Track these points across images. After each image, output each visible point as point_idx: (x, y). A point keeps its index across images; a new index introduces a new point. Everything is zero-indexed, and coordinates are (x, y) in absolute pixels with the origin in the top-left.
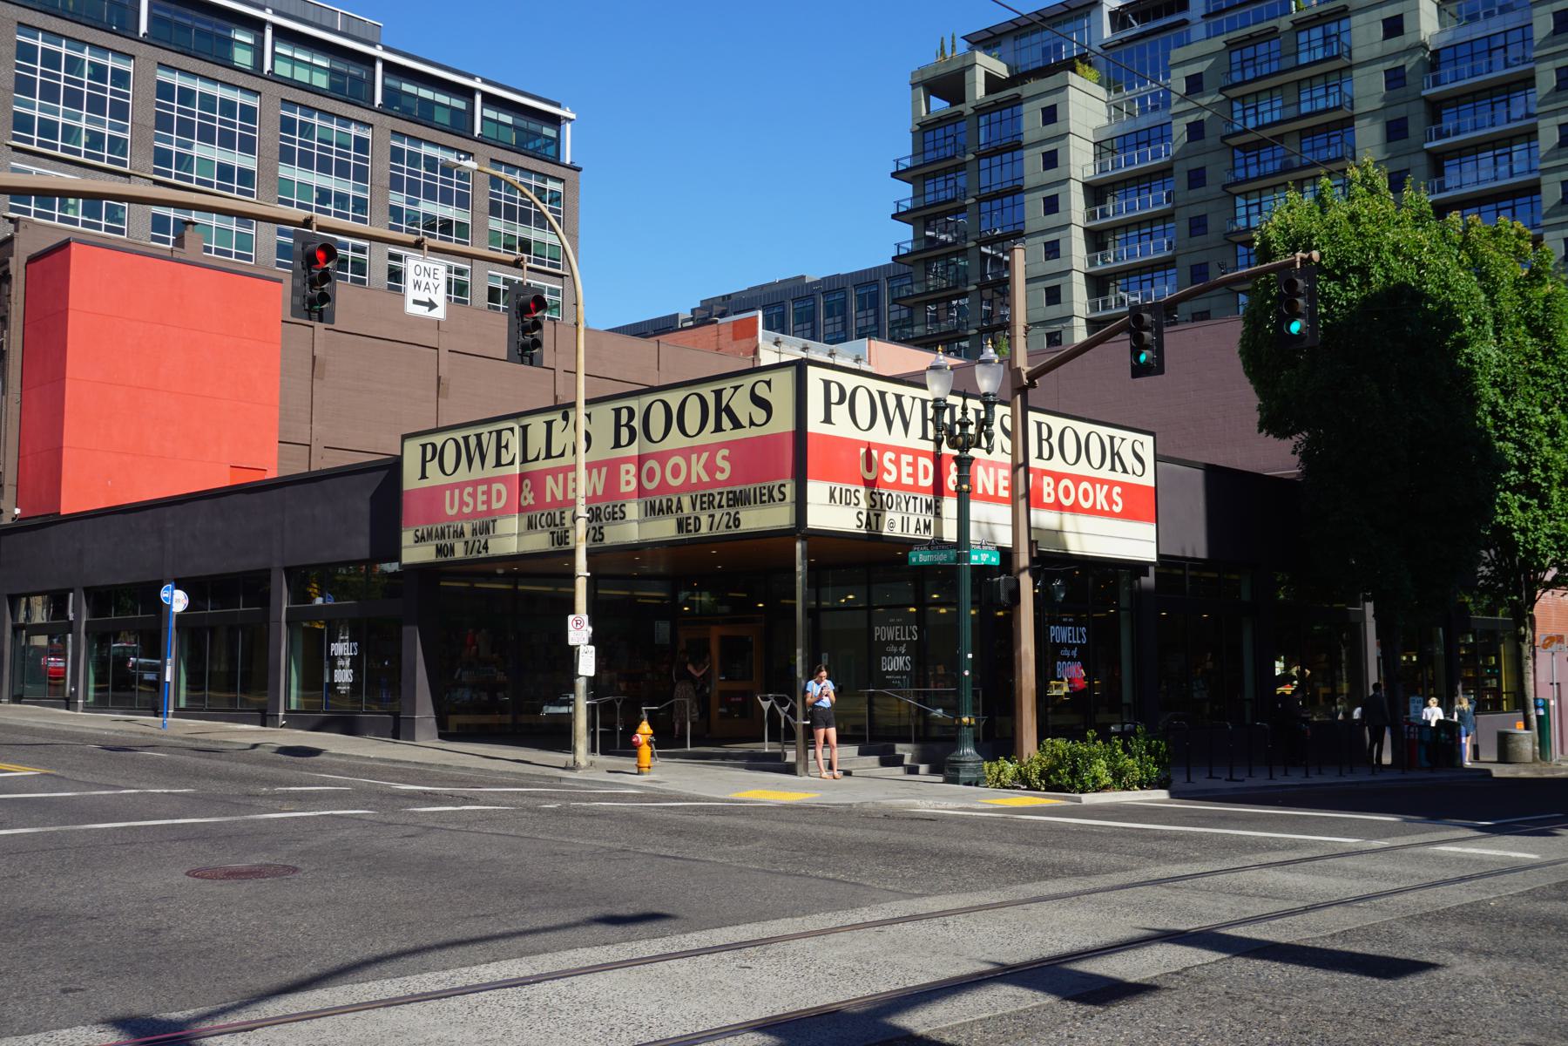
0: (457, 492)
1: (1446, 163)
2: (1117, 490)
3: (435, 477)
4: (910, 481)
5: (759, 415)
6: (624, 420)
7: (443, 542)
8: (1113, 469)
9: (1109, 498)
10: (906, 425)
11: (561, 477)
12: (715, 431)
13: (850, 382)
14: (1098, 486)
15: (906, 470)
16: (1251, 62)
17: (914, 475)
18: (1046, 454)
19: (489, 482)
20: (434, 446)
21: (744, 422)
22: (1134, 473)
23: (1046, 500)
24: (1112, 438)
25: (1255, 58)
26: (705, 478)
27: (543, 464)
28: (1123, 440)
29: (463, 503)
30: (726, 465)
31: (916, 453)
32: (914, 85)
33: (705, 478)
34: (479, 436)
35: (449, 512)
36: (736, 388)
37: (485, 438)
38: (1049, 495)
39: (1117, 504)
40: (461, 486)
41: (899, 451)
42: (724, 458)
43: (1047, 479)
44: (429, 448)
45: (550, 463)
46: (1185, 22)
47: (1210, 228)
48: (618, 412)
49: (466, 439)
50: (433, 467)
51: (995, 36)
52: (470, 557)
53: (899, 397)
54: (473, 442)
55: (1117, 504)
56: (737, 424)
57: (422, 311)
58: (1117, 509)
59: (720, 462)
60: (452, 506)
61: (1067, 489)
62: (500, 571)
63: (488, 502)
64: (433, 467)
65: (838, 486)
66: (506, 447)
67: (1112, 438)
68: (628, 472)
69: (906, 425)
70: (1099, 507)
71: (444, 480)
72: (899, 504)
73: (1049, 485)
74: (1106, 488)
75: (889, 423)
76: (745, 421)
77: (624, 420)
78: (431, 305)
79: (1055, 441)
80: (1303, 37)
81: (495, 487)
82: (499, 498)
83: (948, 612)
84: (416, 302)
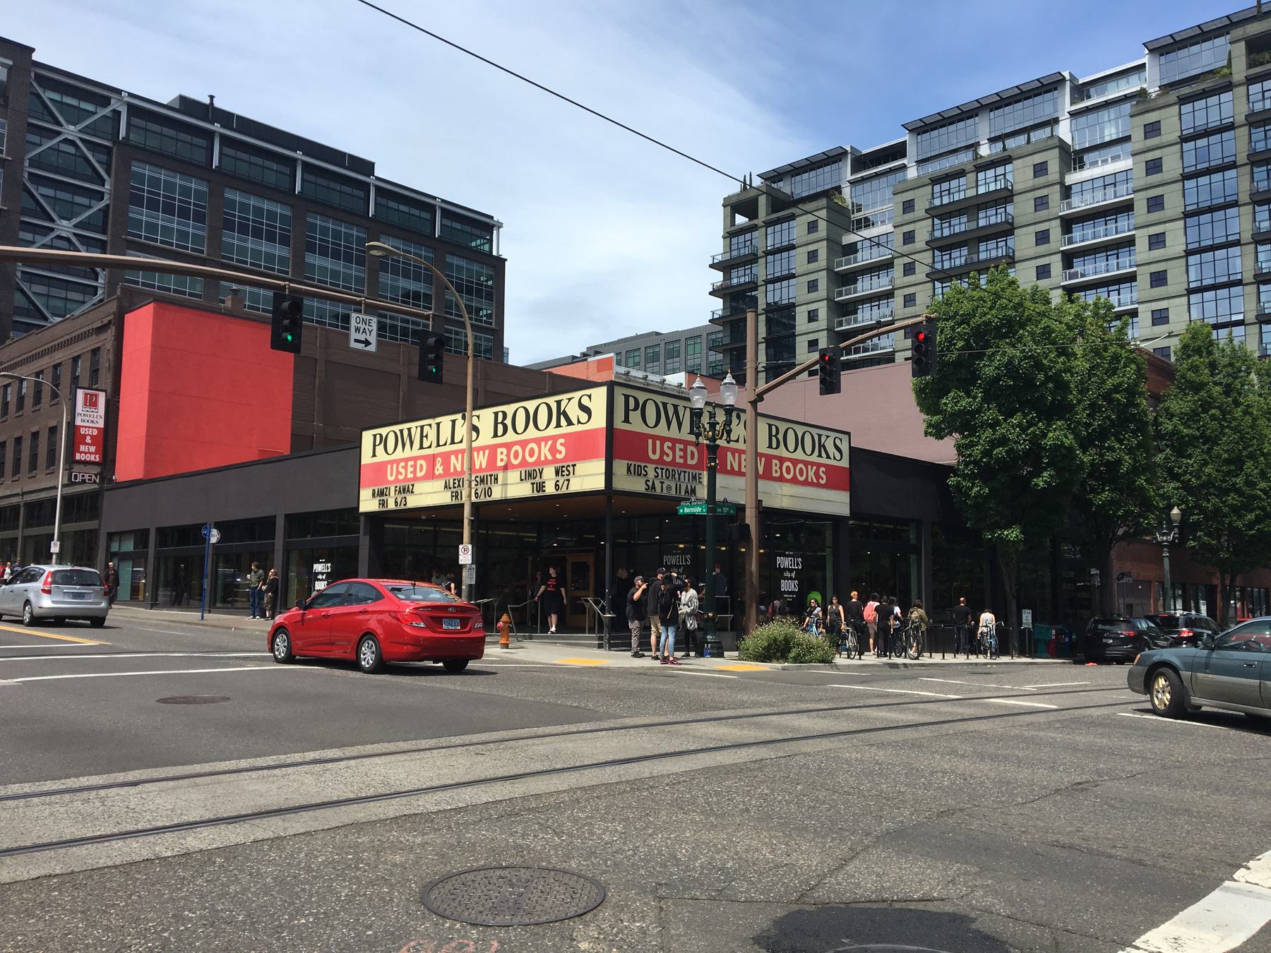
0: (395, 465)
1: (1075, 260)
2: (823, 469)
3: (381, 456)
4: (682, 461)
5: (584, 417)
6: (500, 419)
7: (382, 498)
8: (820, 455)
9: (817, 474)
10: (680, 425)
11: (460, 456)
12: (556, 427)
13: (642, 396)
14: (809, 467)
15: (679, 453)
16: (947, 192)
17: (685, 457)
18: (774, 445)
19: (415, 459)
20: (381, 435)
21: (575, 421)
22: (835, 458)
23: (774, 475)
24: (820, 436)
25: (949, 190)
26: (550, 457)
27: (449, 448)
28: (828, 437)
29: (399, 473)
30: (563, 449)
31: (686, 443)
32: (724, 206)
33: (550, 457)
34: (409, 430)
35: (390, 478)
36: (570, 399)
37: (413, 431)
38: (776, 471)
39: (822, 479)
40: (398, 462)
41: (674, 441)
42: (561, 444)
43: (774, 461)
44: (378, 437)
45: (454, 447)
46: (904, 167)
47: (917, 302)
48: (496, 414)
49: (401, 431)
50: (380, 449)
51: (779, 174)
52: (398, 508)
53: (676, 407)
54: (406, 433)
55: (822, 479)
56: (570, 423)
57: (360, 346)
58: (823, 482)
59: (559, 447)
60: (654, 452)
61: (788, 468)
62: (423, 517)
63: (414, 472)
64: (380, 449)
65: (633, 463)
66: (426, 436)
67: (820, 436)
68: (502, 453)
69: (680, 425)
70: (810, 480)
71: (387, 458)
72: (673, 476)
73: (776, 465)
74: (815, 468)
76: (574, 421)
77: (500, 419)
78: (367, 343)
79: (780, 437)
80: (981, 175)
81: (419, 462)
82: (421, 470)
83: (685, 547)
84: (356, 341)
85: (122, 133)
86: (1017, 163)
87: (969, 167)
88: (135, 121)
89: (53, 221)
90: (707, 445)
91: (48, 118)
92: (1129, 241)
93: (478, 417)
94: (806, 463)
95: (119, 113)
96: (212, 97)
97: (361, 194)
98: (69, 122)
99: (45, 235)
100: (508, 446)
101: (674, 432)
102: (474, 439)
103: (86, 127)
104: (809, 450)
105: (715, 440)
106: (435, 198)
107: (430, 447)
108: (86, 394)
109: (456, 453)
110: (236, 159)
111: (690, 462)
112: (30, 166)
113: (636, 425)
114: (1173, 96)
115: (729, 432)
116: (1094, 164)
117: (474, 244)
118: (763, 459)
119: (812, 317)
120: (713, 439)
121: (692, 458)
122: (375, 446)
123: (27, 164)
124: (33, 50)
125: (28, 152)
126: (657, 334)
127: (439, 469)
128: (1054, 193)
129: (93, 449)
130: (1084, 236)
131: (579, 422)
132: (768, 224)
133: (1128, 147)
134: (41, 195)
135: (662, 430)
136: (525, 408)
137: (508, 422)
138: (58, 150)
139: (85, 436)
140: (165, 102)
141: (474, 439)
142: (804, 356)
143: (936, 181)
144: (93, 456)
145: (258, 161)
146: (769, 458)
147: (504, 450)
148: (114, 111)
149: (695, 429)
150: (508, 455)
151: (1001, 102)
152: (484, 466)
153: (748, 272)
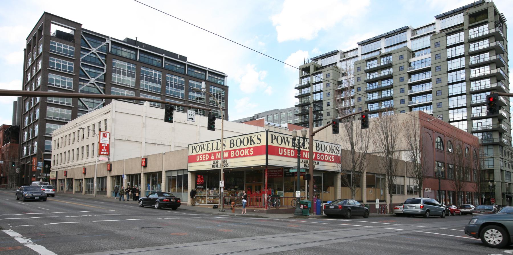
0: (199, 156)
3: (195, 153)
4: (289, 155)
5: (259, 142)
6: (232, 142)
8: (332, 152)
9: (331, 158)
10: (289, 143)
11: (219, 153)
13: (277, 135)
15: (288, 153)
17: (290, 154)
18: (318, 149)
19: (205, 154)
21: (256, 143)
24: (332, 146)
25: (372, 64)
26: (248, 154)
29: (200, 158)
30: (252, 152)
31: (291, 149)
33: (248, 154)
34: (203, 145)
36: (254, 136)
40: (200, 155)
41: (287, 149)
42: (252, 150)
44: (194, 147)
49: (201, 145)
50: (194, 151)
53: (287, 138)
54: (202, 146)
56: (254, 143)
58: (333, 161)
59: (251, 151)
60: (281, 152)
63: (205, 158)
64: (194, 151)
67: (332, 146)
69: (289, 143)
74: (330, 156)
75: (285, 143)
77: (232, 142)
79: (320, 147)
81: (206, 155)
85: (110, 50)
86: (394, 55)
87: (378, 57)
88: (113, 46)
89: (89, 78)
90: (297, 150)
91: (87, 46)
92: (429, 69)
93: (225, 141)
94: (328, 155)
95: (109, 44)
96: (137, 38)
97: (183, 67)
98: (93, 47)
99: (87, 83)
100: (235, 150)
101: (287, 146)
102: (224, 148)
103: (98, 49)
104: (329, 151)
105: (300, 148)
106: (206, 68)
107: (210, 150)
108: (103, 134)
109: (218, 152)
110: (144, 57)
111: (292, 155)
112: (82, 61)
113: (275, 144)
114: (444, 33)
115: (304, 146)
116: (418, 56)
117: (218, 82)
118: (315, 154)
119: (328, 105)
120: (299, 148)
121: (293, 154)
122: (192, 150)
123: (81, 60)
124: (81, 25)
125: (81, 57)
126: (278, 110)
127: (213, 157)
128: (406, 65)
129: (106, 150)
130: (415, 78)
131: (257, 143)
132: (313, 74)
133: (429, 49)
134: (86, 70)
135: (283, 145)
136: (244, 145)
137: (235, 143)
138: (90, 56)
139: (103, 146)
140: (122, 40)
141: (224, 148)
142: (326, 119)
143: (368, 60)
144: (106, 153)
145: (151, 58)
146: (316, 153)
147: (233, 152)
148: (107, 43)
149: (294, 145)
150: (235, 153)
151: (388, 35)
152: (227, 157)
153: (307, 90)
